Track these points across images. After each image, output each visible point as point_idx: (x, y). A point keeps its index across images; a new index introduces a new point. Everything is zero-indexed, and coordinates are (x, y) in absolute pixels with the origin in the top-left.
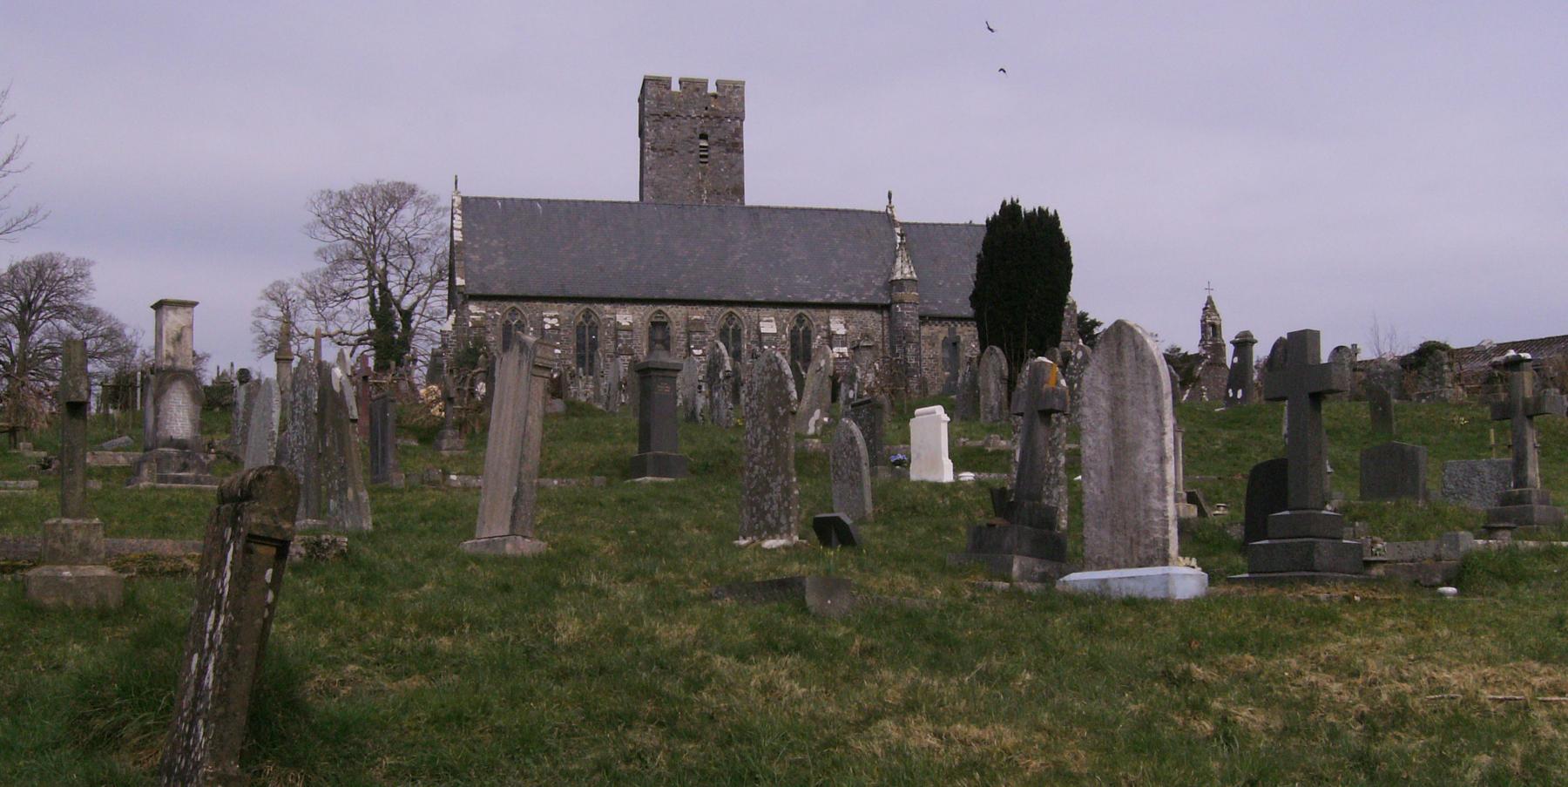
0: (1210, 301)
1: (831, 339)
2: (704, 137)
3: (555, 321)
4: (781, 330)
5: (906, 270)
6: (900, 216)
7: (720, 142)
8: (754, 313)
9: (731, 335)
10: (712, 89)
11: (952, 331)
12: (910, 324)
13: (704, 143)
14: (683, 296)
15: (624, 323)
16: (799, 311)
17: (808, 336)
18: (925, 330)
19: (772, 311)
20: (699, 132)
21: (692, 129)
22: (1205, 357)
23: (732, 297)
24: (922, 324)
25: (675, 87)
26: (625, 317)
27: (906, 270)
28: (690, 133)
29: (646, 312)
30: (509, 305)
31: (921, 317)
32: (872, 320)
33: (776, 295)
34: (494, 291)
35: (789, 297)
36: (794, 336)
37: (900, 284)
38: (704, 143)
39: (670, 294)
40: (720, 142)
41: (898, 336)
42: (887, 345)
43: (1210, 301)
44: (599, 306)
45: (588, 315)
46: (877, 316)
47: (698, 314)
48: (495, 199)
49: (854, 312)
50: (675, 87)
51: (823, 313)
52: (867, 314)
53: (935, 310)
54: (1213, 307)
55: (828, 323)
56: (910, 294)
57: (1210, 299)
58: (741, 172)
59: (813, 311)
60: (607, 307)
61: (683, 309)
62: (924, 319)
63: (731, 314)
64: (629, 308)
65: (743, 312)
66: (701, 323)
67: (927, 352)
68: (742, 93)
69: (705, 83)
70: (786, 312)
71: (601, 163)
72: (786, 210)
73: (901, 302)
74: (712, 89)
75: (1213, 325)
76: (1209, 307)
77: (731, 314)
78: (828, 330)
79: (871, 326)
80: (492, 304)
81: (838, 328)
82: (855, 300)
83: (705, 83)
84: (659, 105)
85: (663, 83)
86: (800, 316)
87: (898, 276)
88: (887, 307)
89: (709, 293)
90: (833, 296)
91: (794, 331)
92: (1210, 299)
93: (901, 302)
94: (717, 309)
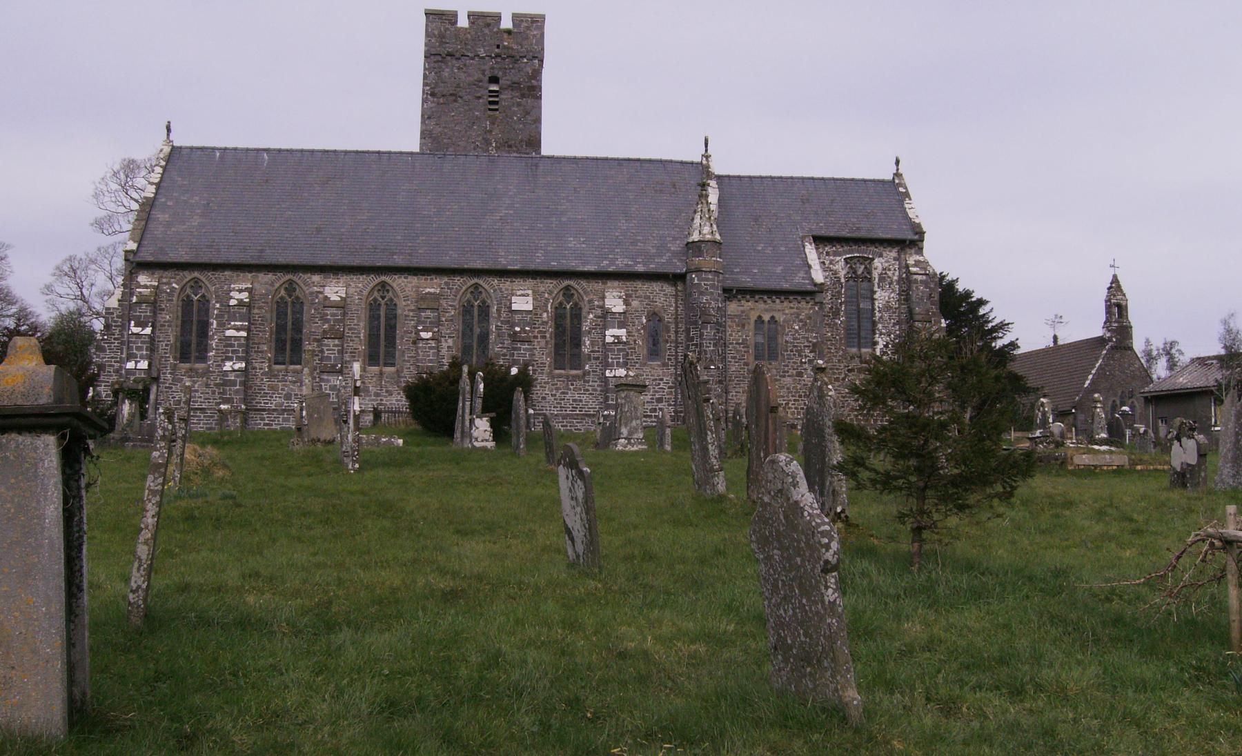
0: (1115, 280)
1: (606, 317)
2: (494, 80)
3: (244, 296)
4: (539, 306)
5: (706, 230)
6: (717, 168)
7: (515, 86)
8: (506, 285)
9: (475, 315)
10: (506, 23)
11: (291, 288)
12: (710, 300)
13: (494, 88)
14: (415, 263)
15: (334, 298)
16: (567, 282)
17: (577, 315)
18: (733, 307)
19: (530, 282)
20: (488, 74)
21: (484, 77)
22: (1110, 339)
23: (478, 265)
24: (728, 299)
25: (463, 22)
26: (335, 290)
27: (706, 230)
28: (477, 76)
29: (362, 285)
30: (189, 275)
31: (725, 290)
32: (662, 295)
33: (538, 263)
34: (172, 257)
35: (554, 265)
36: (559, 316)
37: (695, 248)
38: (494, 88)
39: (399, 261)
40: (515, 86)
41: (694, 317)
42: (682, 327)
43: (1115, 280)
44: (306, 276)
45: (291, 288)
46: (669, 289)
47: (432, 286)
48: (214, 149)
49: (639, 284)
50: (463, 22)
51: (597, 285)
52: (656, 286)
53: (746, 281)
54: (1119, 287)
55: (603, 298)
56: (709, 261)
57: (1115, 276)
58: (538, 120)
59: (584, 283)
60: (316, 278)
61: (414, 280)
62: (730, 293)
63: (476, 286)
64: (344, 279)
65: (491, 285)
66: (436, 297)
67: (734, 334)
68: (541, 28)
69: (497, 17)
70: (549, 284)
71: (384, 112)
72: (574, 160)
73: (698, 271)
74: (506, 23)
75: (1119, 306)
76: (1115, 287)
77: (476, 286)
78: (602, 307)
79: (660, 301)
80: (168, 274)
81: (615, 303)
82: (640, 268)
83: (497, 17)
84: (442, 43)
85: (451, 17)
86: (567, 288)
87: (695, 237)
88: (676, 279)
89: (449, 259)
90: (612, 262)
91: (559, 308)
92: (1115, 276)
93: (698, 271)
94: (458, 280)
